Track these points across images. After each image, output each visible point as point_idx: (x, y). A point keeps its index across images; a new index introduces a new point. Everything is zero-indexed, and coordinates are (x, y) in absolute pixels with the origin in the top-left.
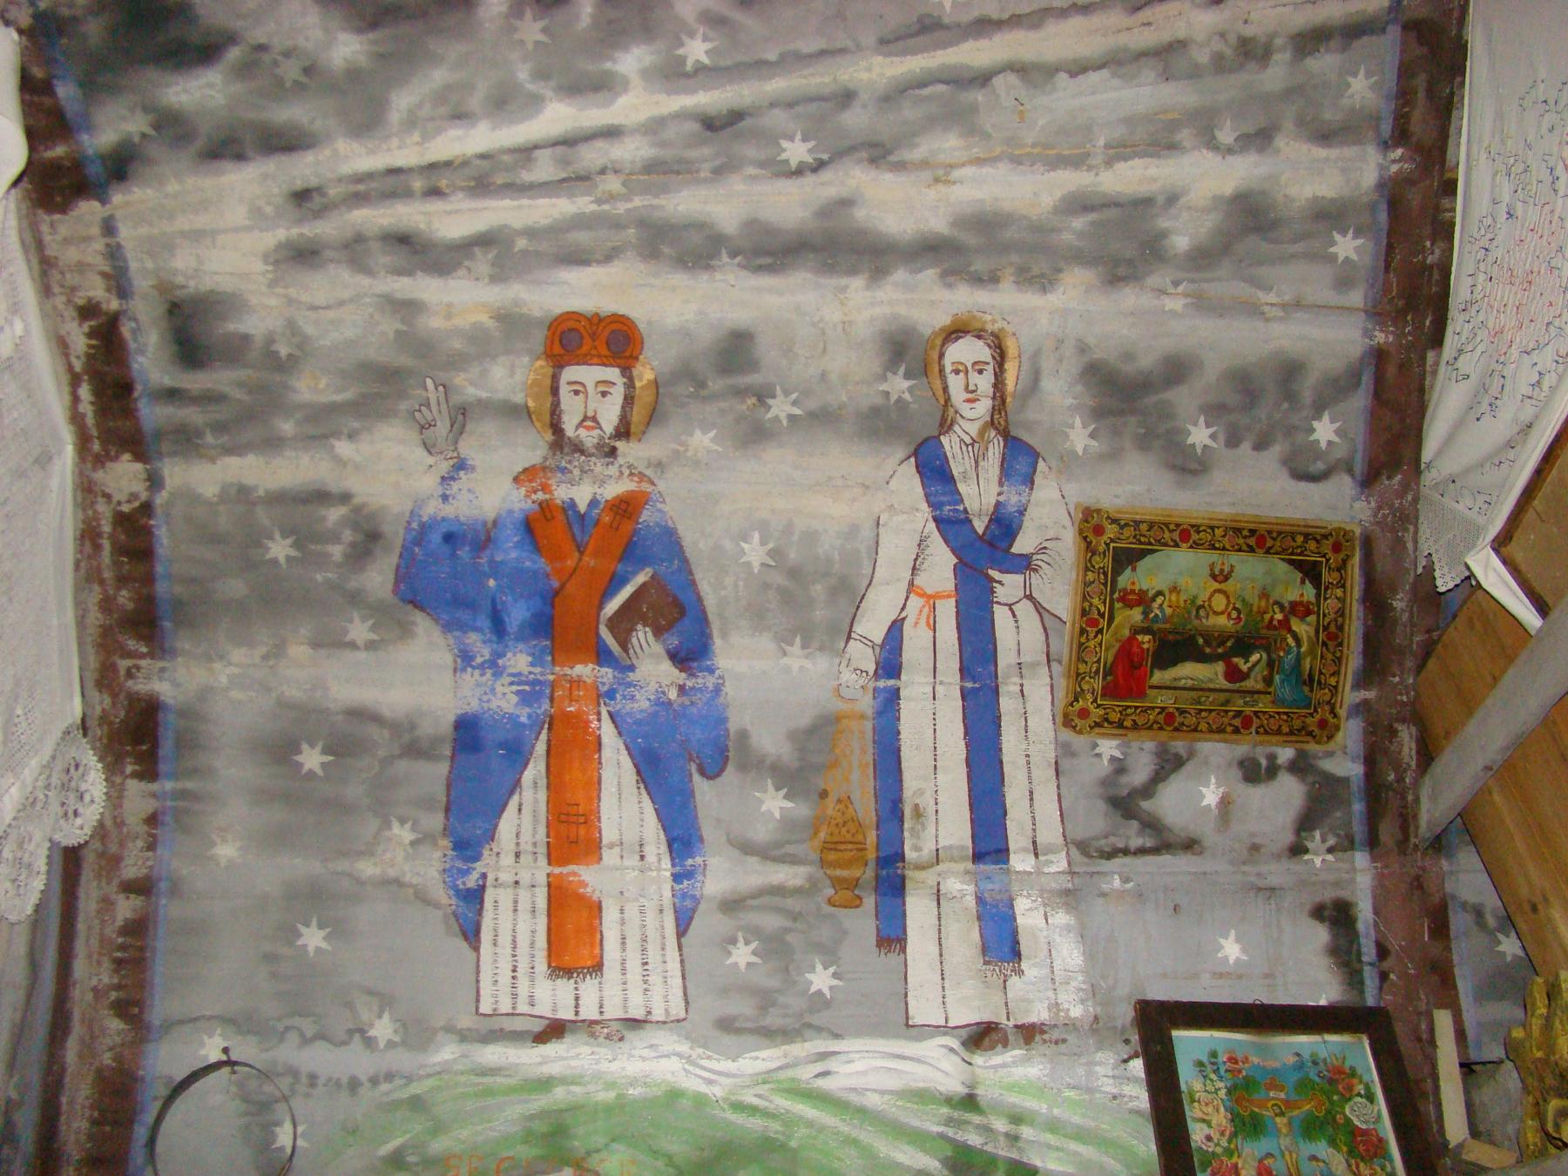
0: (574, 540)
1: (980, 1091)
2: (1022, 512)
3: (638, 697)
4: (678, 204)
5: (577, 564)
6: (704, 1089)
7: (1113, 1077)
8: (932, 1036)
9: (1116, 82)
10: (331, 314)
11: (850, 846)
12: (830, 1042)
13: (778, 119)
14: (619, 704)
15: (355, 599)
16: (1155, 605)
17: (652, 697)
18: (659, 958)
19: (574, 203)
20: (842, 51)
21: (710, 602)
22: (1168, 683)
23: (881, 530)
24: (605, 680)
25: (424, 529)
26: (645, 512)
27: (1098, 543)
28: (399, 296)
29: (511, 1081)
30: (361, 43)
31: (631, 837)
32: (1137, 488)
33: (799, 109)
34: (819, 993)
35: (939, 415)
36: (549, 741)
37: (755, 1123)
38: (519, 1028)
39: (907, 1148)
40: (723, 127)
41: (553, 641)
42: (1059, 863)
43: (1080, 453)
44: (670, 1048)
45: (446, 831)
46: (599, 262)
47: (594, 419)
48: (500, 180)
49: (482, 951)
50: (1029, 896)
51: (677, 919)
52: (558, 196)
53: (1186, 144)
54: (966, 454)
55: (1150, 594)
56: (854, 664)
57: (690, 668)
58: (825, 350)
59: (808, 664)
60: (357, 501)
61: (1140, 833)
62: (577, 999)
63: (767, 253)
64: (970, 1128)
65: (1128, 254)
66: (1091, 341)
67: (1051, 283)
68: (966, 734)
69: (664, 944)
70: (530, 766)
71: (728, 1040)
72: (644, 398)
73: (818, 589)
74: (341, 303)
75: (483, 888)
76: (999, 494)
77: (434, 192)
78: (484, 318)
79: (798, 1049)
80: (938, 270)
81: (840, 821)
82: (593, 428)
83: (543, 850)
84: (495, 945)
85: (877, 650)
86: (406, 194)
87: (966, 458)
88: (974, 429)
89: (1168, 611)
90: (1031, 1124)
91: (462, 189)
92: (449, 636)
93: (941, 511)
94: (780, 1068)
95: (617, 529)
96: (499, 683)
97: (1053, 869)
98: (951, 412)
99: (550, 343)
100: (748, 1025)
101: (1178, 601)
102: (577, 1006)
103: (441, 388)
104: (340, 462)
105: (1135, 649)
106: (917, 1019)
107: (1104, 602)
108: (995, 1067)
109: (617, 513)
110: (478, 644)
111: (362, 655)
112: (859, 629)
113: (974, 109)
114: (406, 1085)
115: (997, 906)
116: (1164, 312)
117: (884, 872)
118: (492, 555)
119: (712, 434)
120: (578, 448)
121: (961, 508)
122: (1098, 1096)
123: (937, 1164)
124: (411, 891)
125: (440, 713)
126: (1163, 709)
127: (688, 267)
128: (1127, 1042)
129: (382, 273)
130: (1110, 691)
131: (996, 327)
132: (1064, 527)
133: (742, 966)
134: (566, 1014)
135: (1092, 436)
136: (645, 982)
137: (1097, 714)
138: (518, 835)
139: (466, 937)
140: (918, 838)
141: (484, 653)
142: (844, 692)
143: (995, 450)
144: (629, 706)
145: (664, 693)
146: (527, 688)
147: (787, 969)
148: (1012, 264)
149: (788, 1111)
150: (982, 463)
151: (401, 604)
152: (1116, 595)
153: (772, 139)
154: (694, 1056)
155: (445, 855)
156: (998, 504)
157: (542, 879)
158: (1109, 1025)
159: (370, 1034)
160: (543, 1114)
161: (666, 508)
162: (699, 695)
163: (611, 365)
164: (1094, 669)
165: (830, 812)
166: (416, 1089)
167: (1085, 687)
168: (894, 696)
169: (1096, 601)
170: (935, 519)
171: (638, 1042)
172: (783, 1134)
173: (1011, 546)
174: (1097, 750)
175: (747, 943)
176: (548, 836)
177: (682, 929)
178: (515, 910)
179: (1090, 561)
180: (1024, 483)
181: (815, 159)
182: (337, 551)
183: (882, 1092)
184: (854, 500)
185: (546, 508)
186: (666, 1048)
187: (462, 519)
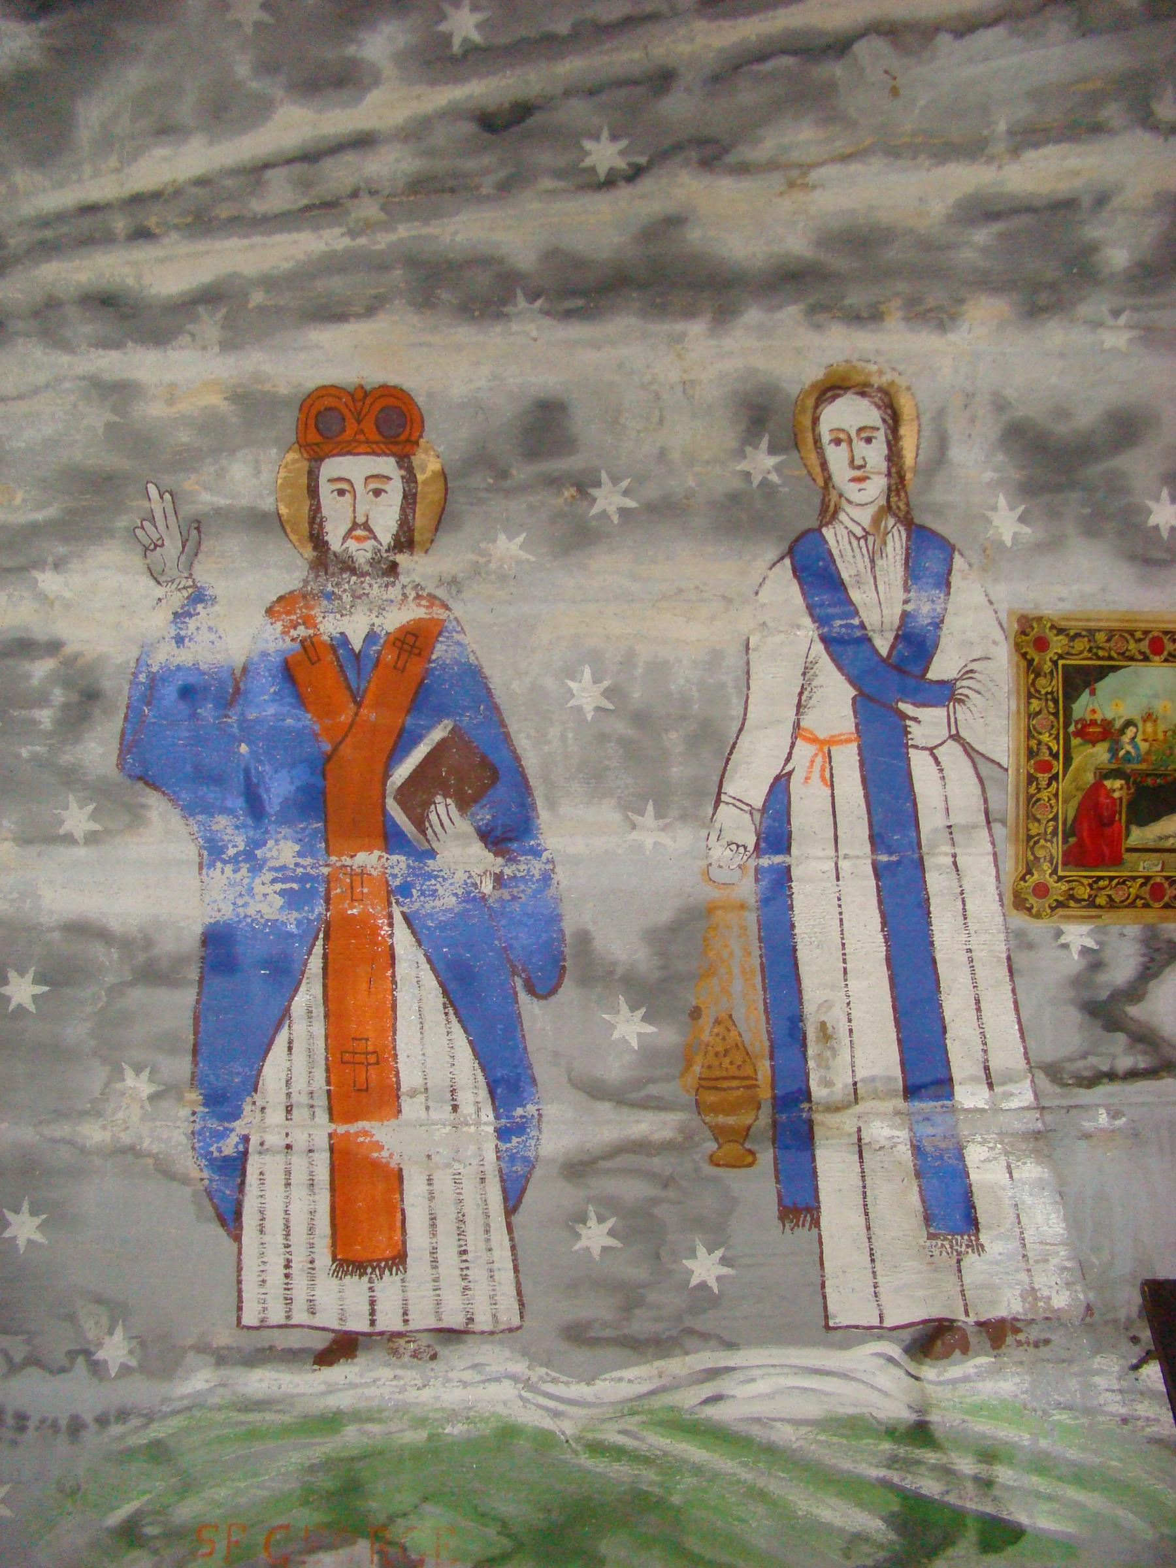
0: (349, 687)
1: (934, 1417)
2: (938, 624)
3: (441, 892)
4: (456, 233)
5: (353, 720)
6: (548, 1423)
7: (1121, 1391)
8: (861, 1341)
9: (1015, 42)
10: (21, 407)
11: (735, 1083)
12: (723, 1354)
13: (577, 111)
14: (415, 903)
15: (71, 778)
16: (1126, 739)
17: (460, 892)
18: (482, 1245)
19: (321, 237)
20: (652, 17)
21: (531, 762)
22: (1151, 845)
23: (752, 655)
24: (396, 871)
25: (155, 681)
26: (439, 647)
27: (1044, 661)
28: (107, 377)
29: (287, 1418)
30: (30, 35)
31: (438, 1080)
32: (1088, 588)
33: (604, 97)
34: (703, 1286)
35: (817, 501)
36: (325, 957)
37: (620, 1471)
38: (296, 1345)
39: (833, 1501)
40: (506, 127)
41: (326, 821)
42: (1022, 1095)
43: (1009, 543)
44: (501, 1369)
45: (196, 1080)
46: (359, 316)
47: (366, 526)
48: (224, 211)
49: (244, 1240)
50: (983, 1142)
51: (505, 1191)
52: (298, 229)
53: (1115, 123)
54: (857, 551)
55: (1118, 724)
56: (727, 836)
57: (508, 851)
58: (661, 421)
59: (665, 839)
60: (68, 650)
61: (1130, 1048)
62: (372, 1303)
63: (573, 293)
64: (922, 1470)
65: (1050, 275)
66: (1009, 393)
67: (953, 318)
68: (884, 924)
69: (488, 1225)
70: (303, 989)
71: (580, 1355)
72: (429, 495)
73: (674, 739)
74: (36, 391)
75: (245, 1154)
76: (906, 602)
77: (143, 234)
78: (216, 400)
79: (677, 1366)
80: (802, 306)
81: (720, 1049)
82: (366, 538)
83: (322, 1101)
84: (261, 1232)
85: (757, 816)
86: (107, 239)
87: (859, 557)
88: (865, 517)
89: (1144, 746)
90: (1010, 1461)
91: (177, 228)
92: (191, 821)
93: (831, 626)
94: (653, 1393)
95: (404, 670)
96: (258, 881)
97: (1014, 1104)
98: (834, 497)
99: (303, 425)
100: (608, 1333)
101: (1155, 732)
102: (373, 1312)
103: (167, 496)
104: (45, 600)
105: (1103, 800)
106: (840, 1317)
107: (1057, 738)
108: (954, 1382)
109: (401, 649)
110: (229, 831)
111: (81, 852)
112: (730, 789)
113: (830, 87)
114: (146, 1426)
115: (941, 1157)
116: (1103, 351)
117: (784, 1116)
118: (242, 714)
119: (520, 539)
120: (348, 566)
121: (856, 622)
122: (1101, 1418)
123: (880, 1524)
124: (151, 1161)
125: (182, 924)
126: (1148, 878)
127: (473, 318)
128: (1135, 1340)
129: (84, 347)
130: (1076, 857)
131: (884, 380)
132: (995, 643)
133: (596, 1252)
134: (359, 1325)
135: (1022, 519)
136: (464, 1278)
137: (1058, 889)
138: (288, 1082)
139: (222, 1220)
140: (828, 1068)
141: (237, 842)
142: (715, 873)
143: (896, 543)
144: (430, 905)
145: (475, 885)
146: (295, 886)
147: (658, 1256)
148: (897, 294)
149: (665, 1453)
150: (879, 562)
151: (129, 782)
152: (1072, 729)
153: (571, 138)
154: (534, 1379)
155: (194, 1113)
156: (905, 615)
157: (322, 1142)
158: (1109, 1317)
159: (95, 1357)
160: (328, 1465)
161: (466, 640)
162: (523, 887)
163: (386, 455)
164: (1050, 830)
165: (706, 1036)
166: (156, 1431)
167: (1040, 853)
168: (783, 877)
169: (1045, 738)
170: (824, 639)
171: (457, 1359)
172: (661, 1485)
173: (926, 670)
174: (1063, 940)
175: (601, 1219)
176: (328, 1083)
177: (511, 1204)
178: (288, 1185)
179: (1033, 684)
180: (937, 585)
181: (629, 164)
182: (45, 717)
183: (797, 1423)
184: (713, 618)
185: (309, 647)
186: (495, 1368)
187: (203, 667)
